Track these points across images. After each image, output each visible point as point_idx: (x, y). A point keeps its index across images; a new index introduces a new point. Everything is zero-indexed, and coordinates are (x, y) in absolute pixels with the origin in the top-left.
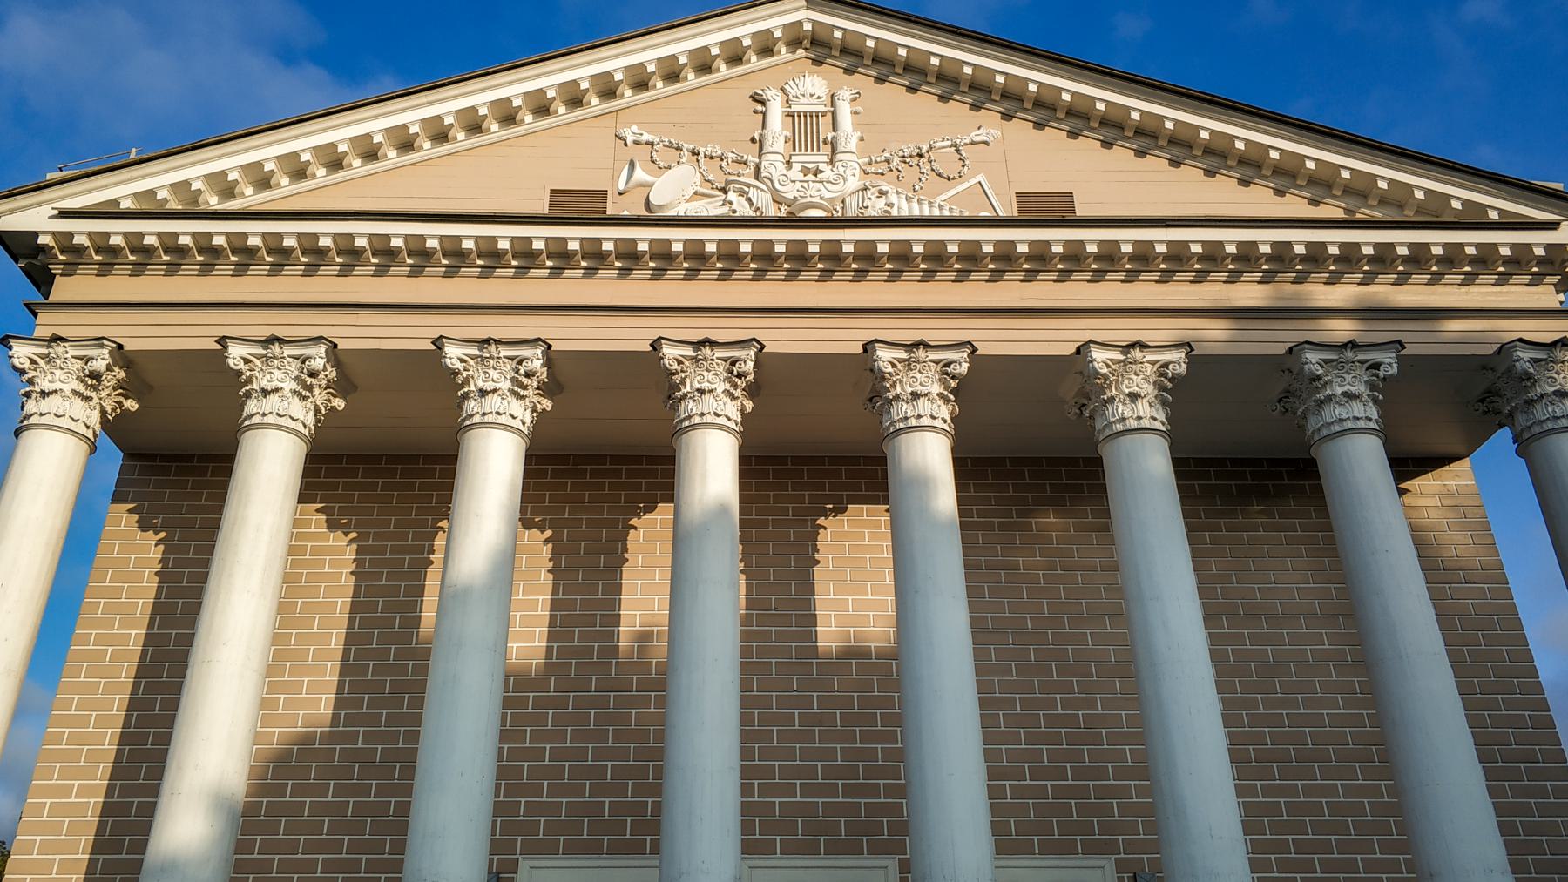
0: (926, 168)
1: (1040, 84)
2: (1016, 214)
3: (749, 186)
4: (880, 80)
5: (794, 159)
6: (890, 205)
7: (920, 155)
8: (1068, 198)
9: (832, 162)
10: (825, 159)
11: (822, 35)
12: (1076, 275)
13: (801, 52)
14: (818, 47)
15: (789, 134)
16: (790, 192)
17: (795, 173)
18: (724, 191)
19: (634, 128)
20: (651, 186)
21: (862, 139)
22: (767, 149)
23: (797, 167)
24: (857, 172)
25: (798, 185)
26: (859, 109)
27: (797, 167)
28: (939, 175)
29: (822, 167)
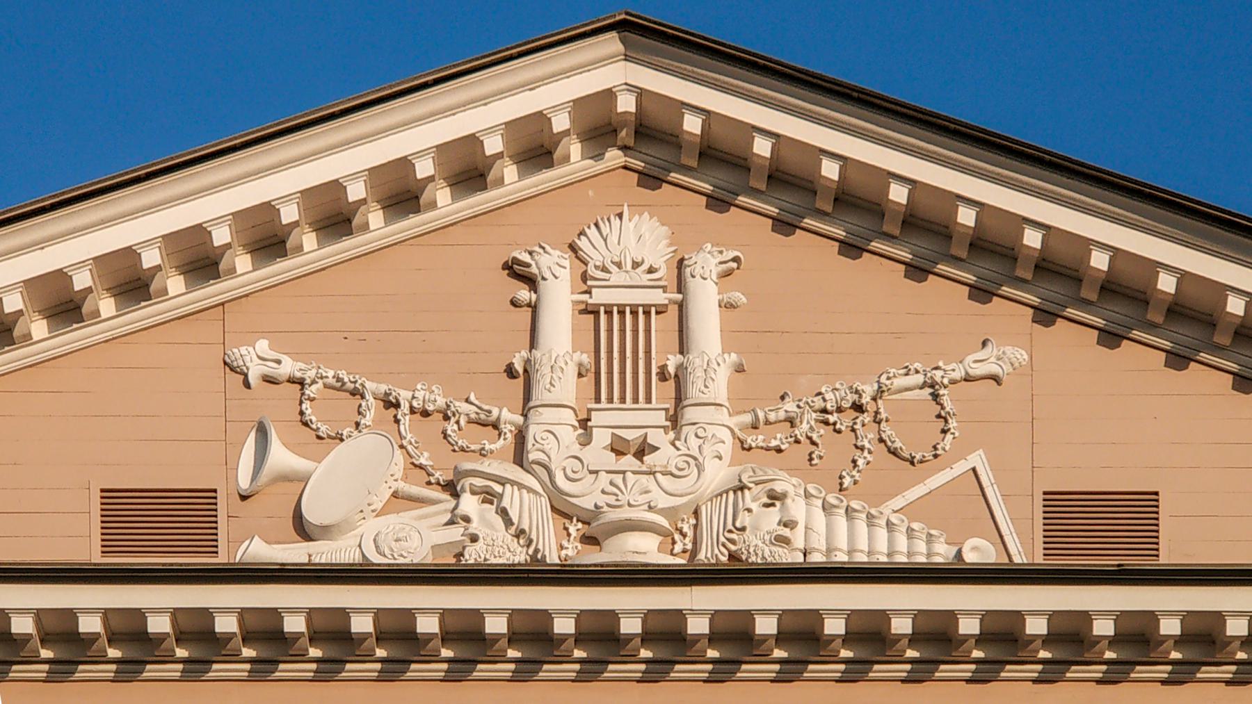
0: (868, 438)
1: (1116, 253)
2: (1039, 559)
3: (502, 481)
4: (784, 226)
5: (596, 418)
6: (789, 524)
7: (858, 408)
8: (1142, 507)
9: (675, 421)
10: (660, 418)
11: (659, 117)
12: (1140, 672)
13: (614, 157)
14: (650, 145)
15: (587, 359)
16: (587, 495)
17: (598, 453)
18: (451, 488)
19: (263, 346)
20: (304, 479)
21: (740, 369)
22: (540, 395)
23: (602, 438)
24: (727, 448)
25: (604, 478)
26: (739, 297)
27: (602, 438)
28: (894, 452)
29: (655, 437)
